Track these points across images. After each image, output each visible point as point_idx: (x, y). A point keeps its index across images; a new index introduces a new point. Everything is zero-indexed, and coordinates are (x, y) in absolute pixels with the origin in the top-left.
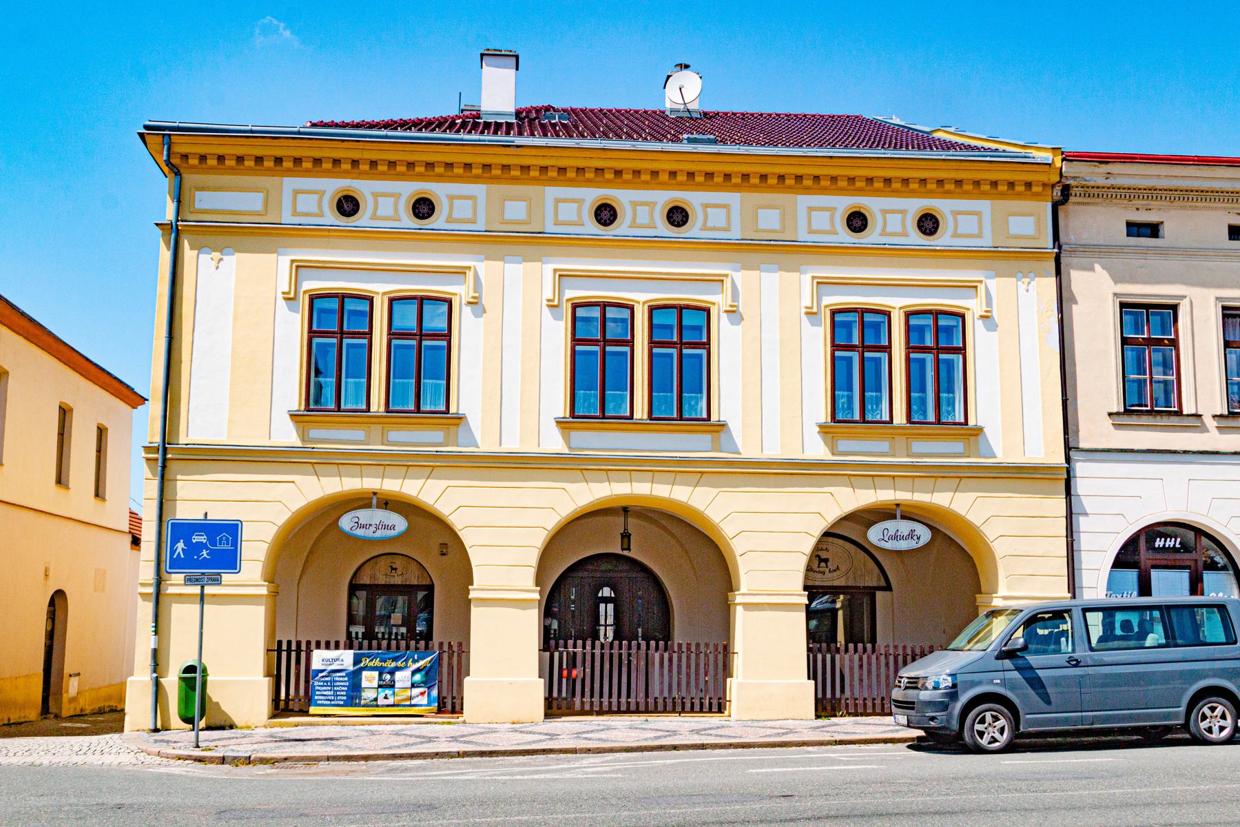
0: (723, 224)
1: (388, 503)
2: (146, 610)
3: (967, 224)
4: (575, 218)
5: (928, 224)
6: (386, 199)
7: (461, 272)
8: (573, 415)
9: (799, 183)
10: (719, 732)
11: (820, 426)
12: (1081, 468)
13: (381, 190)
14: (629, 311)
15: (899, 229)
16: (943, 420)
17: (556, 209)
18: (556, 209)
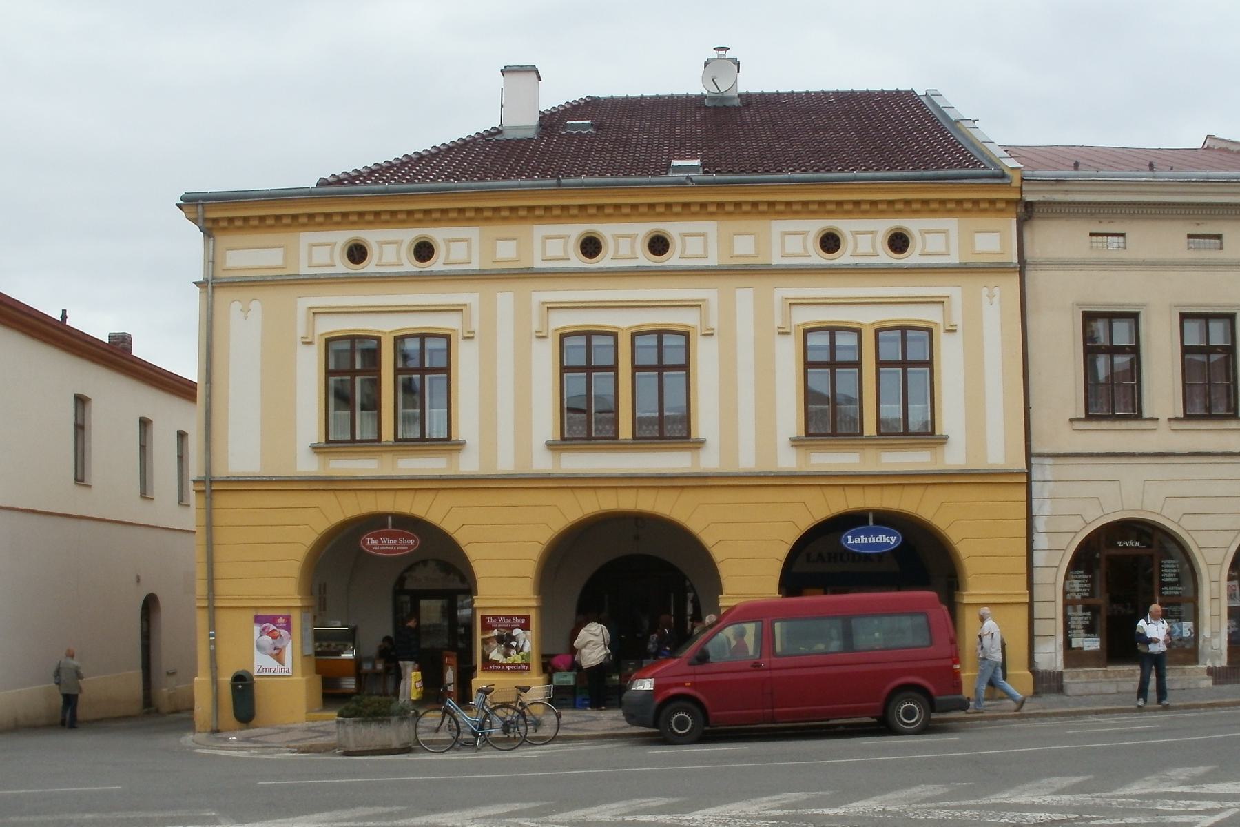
0: (701, 252)
1: (886, 520)
2: (202, 620)
3: (694, 246)
4: (801, 251)
5: (659, 245)
6: (390, 247)
7: (457, 309)
8: (807, 434)
9: (533, 214)
10: (580, 726)
11: (792, 440)
12: (1043, 472)
13: (315, 241)
14: (855, 336)
15: (869, 250)
16: (839, 431)
17: (310, 253)
18: (310, 253)
